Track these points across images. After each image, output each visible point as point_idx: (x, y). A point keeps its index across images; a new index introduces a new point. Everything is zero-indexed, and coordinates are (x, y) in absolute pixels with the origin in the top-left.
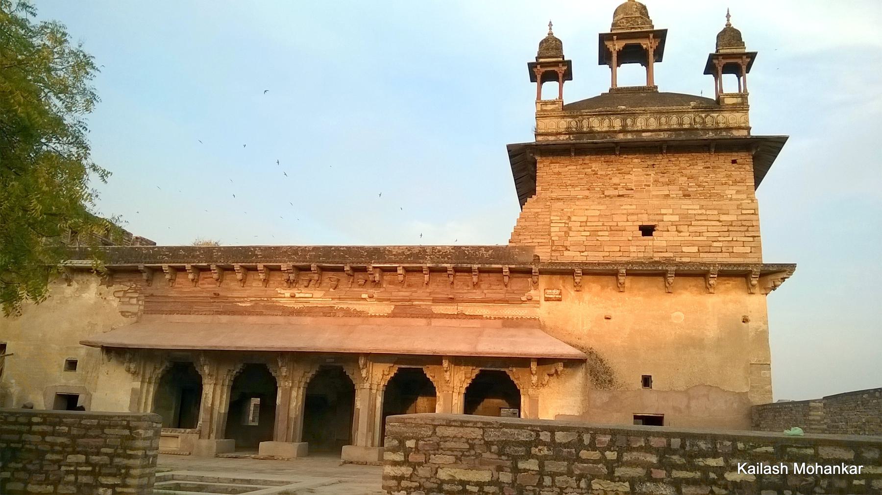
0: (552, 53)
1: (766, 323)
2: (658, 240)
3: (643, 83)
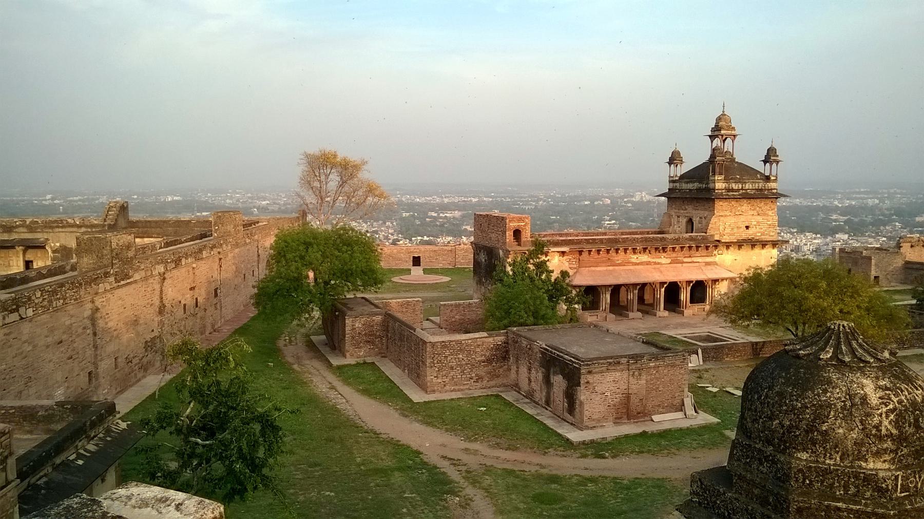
2: (751, 231)
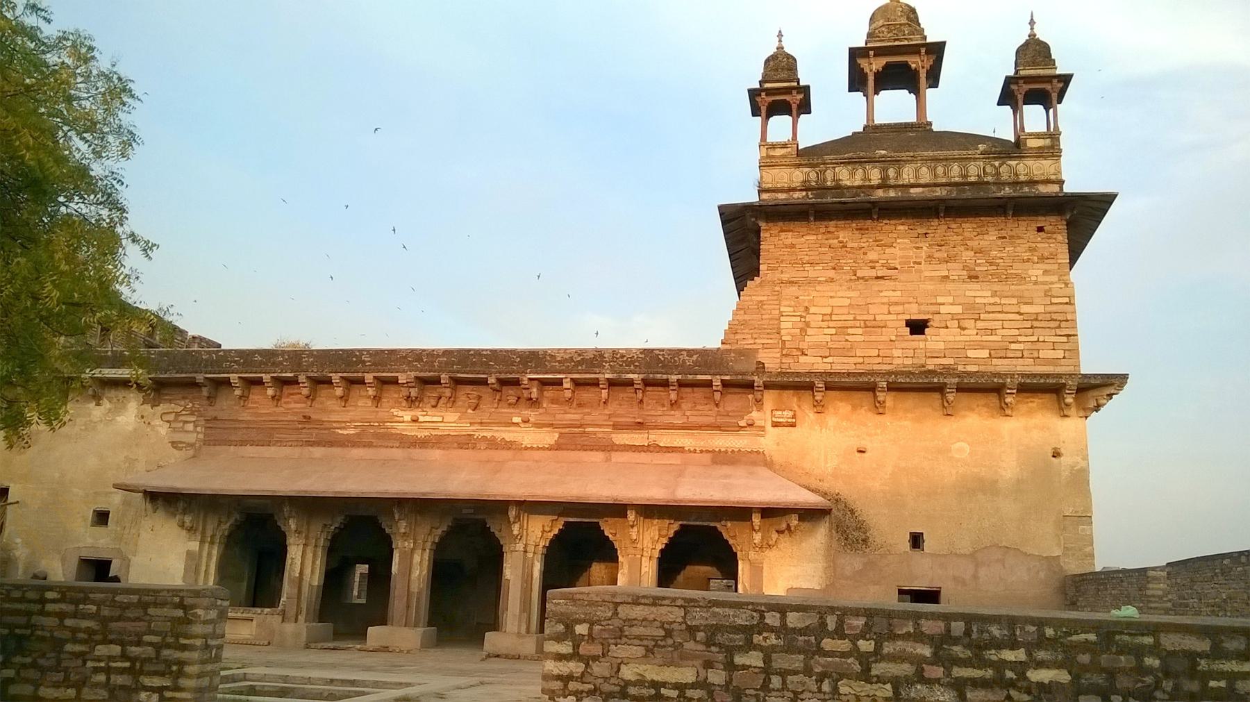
0: (783, 75)
1: (1086, 458)
2: (933, 340)
3: (911, 118)
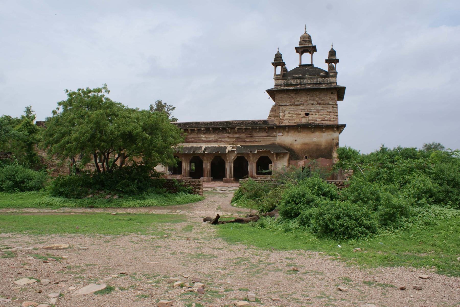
0: (279, 59)
1: (338, 140)
3: (310, 63)
